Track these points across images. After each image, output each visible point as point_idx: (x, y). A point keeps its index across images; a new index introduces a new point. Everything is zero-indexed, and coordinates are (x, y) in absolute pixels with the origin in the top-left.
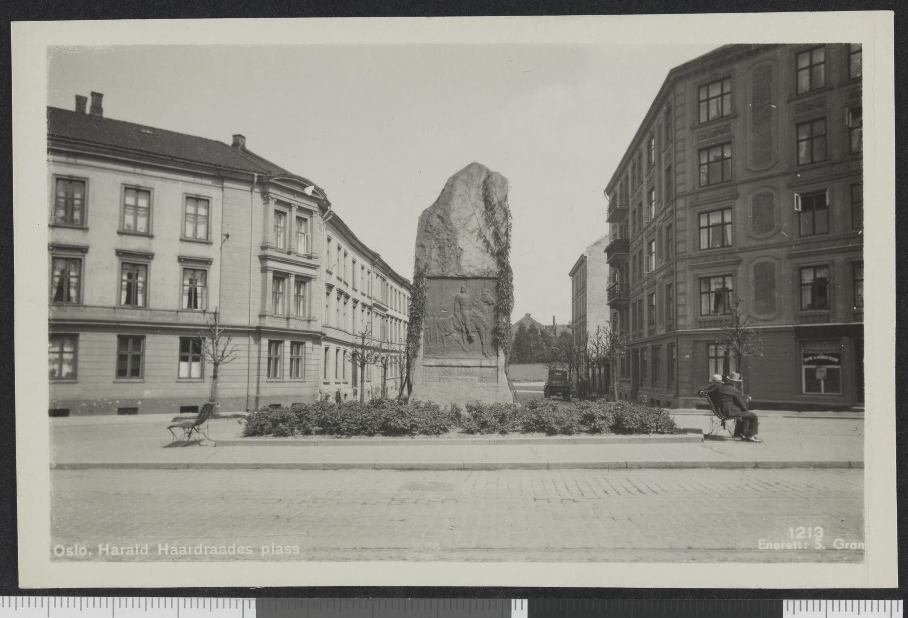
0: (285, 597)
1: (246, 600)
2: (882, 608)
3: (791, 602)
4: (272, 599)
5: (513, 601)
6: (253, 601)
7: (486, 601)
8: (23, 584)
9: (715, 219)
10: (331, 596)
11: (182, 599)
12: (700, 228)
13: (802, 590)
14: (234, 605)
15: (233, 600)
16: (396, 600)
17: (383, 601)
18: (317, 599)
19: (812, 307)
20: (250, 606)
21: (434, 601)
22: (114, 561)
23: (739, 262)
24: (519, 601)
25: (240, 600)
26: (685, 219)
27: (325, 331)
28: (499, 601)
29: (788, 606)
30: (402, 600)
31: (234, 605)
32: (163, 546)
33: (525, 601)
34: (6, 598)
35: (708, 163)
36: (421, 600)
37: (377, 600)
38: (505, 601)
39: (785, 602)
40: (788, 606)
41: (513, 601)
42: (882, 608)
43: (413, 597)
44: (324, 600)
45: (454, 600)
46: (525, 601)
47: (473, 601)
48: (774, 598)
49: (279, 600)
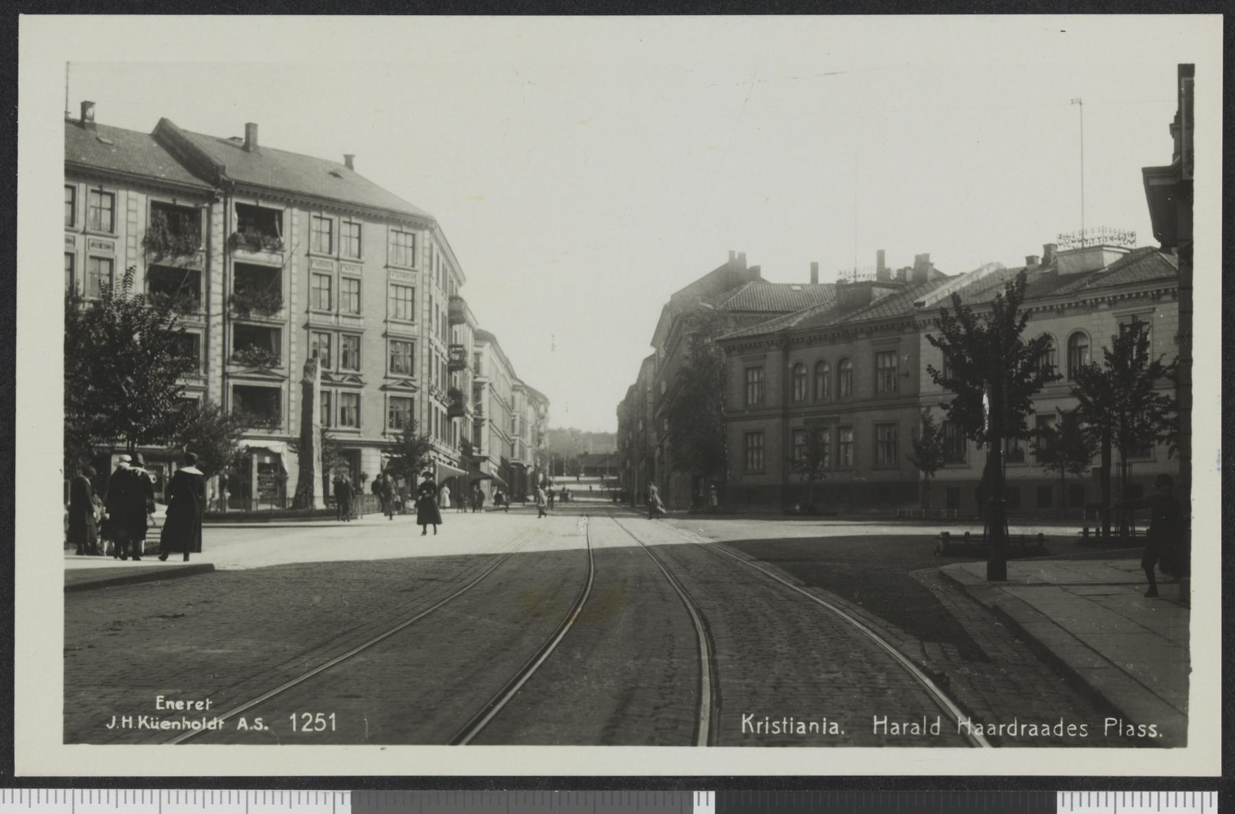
4: (373, 792)
5: (695, 793)
7: (660, 793)
10: (451, 788)
16: (538, 793)
17: (521, 793)
24: (703, 794)
28: (677, 793)
30: (547, 793)
33: (712, 794)
37: (513, 793)
38: (685, 793)
41: (695, 793)
43: (562, 788)
45: (616, 793)
46: (712, 794)
47: (642, 793)
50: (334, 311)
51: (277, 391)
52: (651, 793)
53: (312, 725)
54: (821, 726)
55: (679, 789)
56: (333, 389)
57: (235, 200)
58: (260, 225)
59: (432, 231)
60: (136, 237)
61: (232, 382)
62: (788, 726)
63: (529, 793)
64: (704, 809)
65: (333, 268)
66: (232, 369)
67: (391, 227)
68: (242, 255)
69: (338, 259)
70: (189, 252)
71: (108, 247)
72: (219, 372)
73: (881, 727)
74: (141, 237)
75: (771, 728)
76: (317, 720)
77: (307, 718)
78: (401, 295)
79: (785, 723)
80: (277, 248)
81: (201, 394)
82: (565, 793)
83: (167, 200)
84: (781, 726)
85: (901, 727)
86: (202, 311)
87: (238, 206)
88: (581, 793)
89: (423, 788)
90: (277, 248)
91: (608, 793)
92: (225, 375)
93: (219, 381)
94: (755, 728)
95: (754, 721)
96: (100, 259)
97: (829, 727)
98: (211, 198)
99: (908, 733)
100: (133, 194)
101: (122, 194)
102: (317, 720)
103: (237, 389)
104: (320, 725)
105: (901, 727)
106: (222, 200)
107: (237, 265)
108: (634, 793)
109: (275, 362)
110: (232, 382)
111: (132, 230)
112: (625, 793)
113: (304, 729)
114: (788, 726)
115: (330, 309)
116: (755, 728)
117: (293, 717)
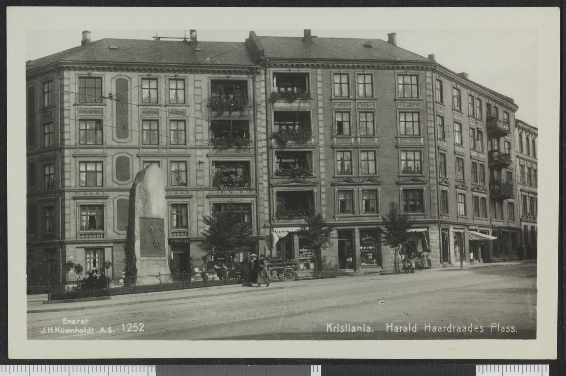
0: (174, 365)
1: (150, 367)
2: (532, 369)
3: (481, 366)
4: (166, 366)
5: (312, 366)
6: (154, 367)
7: (296, 366)
8: (12, 356)
9: (90, 168)
10: (201, 364)
11: (51, 366)
12: (80, 172)
13: (52, 360)
14: (142, 370)
15: (142, 367)
16: (241, 366)
17: (233, 367)
18: (193, 366)
19: (177, 226)
20: (152, 371)
21: (265, 367)
22: (132, 338)
23: (106, 198)
24: (316, 366)
25: (146, 367)
26: (70, 164)
27: (486, 151)
28: (304, 366)
29: (479, 368)
30: (245, 366)
31: (142, 370)
32: (50, 331)
33: (320, 367)
34: (4, 366)
35: (86, 130)
36: (256, 366)
37: (229, 366)
38: (307, 366)
39: (477, 366)
40: (479, 368)
41: (312, 366)
42: (532, 369)
43: (251, 364)
44: (201, 367)
45: (276, 366)
46: (320, 367)
47: (288, 366)
48: (469, 366)
49: (170, 367)
50: (353, 135)
51: (311, 193)
52: (292, 366)
53: (132, 329)
54: (363, 328)
55: (304, 364)
56: (355, 189)
57: (273, 70)
58: (294, 83)
59: (433, 70)
60: (201, 104)
61: (275, 190)
62: (348, 329)
63: (237, 367)
64: (316, 374)
65: (352, 106)
66: (274, 181)
67: (398, 72)
68: (281, 105)
69: (355, 100)
70: (240, 108)
71: (155, 113)
72: (266, 184)
73: (390, 328)
74: (204, 104)
75: (340, 329)
76: (134, 326)
77: (130, 325)
78: (409, 118)
79: (346, 327)
80: (306, 97)
81: (254, 199)
82: (253, 366)
83: (223, 76)
84: (344, 328)
85: (399, 328)
86: (252, 145)
87: (274, 74)
88: (260, 366)
89: (188, 364)
90: (306, 97)
91: (272, 366)
92: (270, 186)
93: (266, 191)
94: (333, 328)
95: (332, 327)
96: (177, 121)
97: (366, 328)
98: (253, 72)
99: (402, 331)
100: (198, 76)
101: (190, 77)
102: (134, 326)
103: (279, 194)
104: (135, 329)
105: (399, 328)
106: (263, 72)
107: (275, 113)
108: (284, 366)
109: (309, 175)
110: (275, 190)
111: (198, 100)
112: (280, 366)
113: (128, 331)
114: (348, 329)
115: (350, 134)
116: (333, 328)
117: (123, 325)
